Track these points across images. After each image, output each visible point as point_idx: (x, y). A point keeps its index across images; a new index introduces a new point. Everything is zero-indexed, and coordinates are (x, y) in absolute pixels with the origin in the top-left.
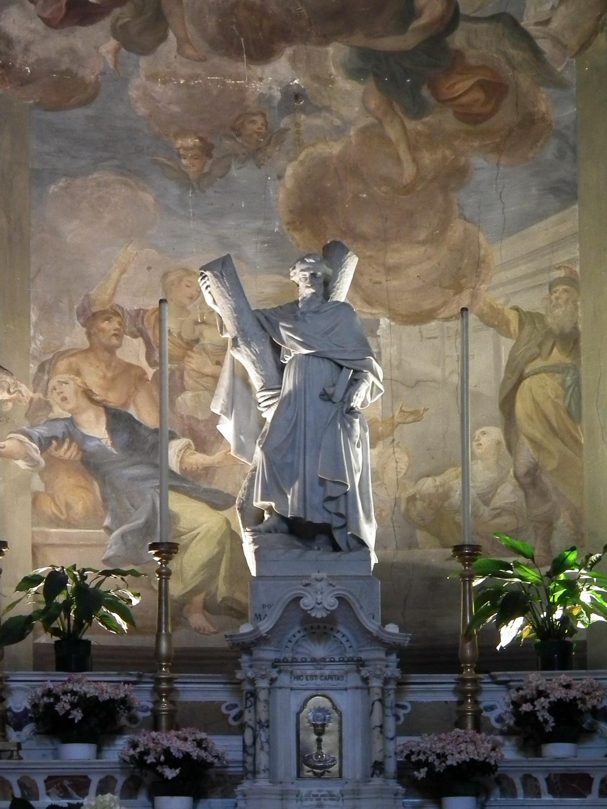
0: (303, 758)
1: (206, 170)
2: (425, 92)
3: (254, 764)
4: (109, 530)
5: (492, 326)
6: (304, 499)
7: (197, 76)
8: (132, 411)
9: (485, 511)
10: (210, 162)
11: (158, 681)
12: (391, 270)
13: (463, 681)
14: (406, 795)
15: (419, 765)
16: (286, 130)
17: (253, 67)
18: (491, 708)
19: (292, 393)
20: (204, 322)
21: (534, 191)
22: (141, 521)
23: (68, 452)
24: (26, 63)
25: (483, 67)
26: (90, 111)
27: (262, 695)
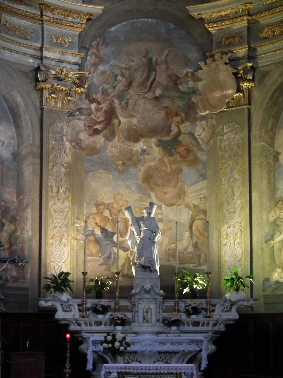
0: (144, 318)
1: (124, 169)
2: (173, 151)
3: (135, 319)
4: (101, 257)
5: (188, 208)
6: (145, 261)
7: (122, 146)
8: (106, 228)
9: (185, 253)
10: (124, 167)
11: (116, 301)
12: (165, 193)
13: (175, 302)
14: (164, 326)
15: (166, 320)
16: (141, 159)
17: (135, 144)
18: (181, 307)
20: (123, 206)
21: (197, 175)
22: (108, 255)
23: (92, 238)
25: (187, 145)
26: (98, 155)
27: (136, 305)
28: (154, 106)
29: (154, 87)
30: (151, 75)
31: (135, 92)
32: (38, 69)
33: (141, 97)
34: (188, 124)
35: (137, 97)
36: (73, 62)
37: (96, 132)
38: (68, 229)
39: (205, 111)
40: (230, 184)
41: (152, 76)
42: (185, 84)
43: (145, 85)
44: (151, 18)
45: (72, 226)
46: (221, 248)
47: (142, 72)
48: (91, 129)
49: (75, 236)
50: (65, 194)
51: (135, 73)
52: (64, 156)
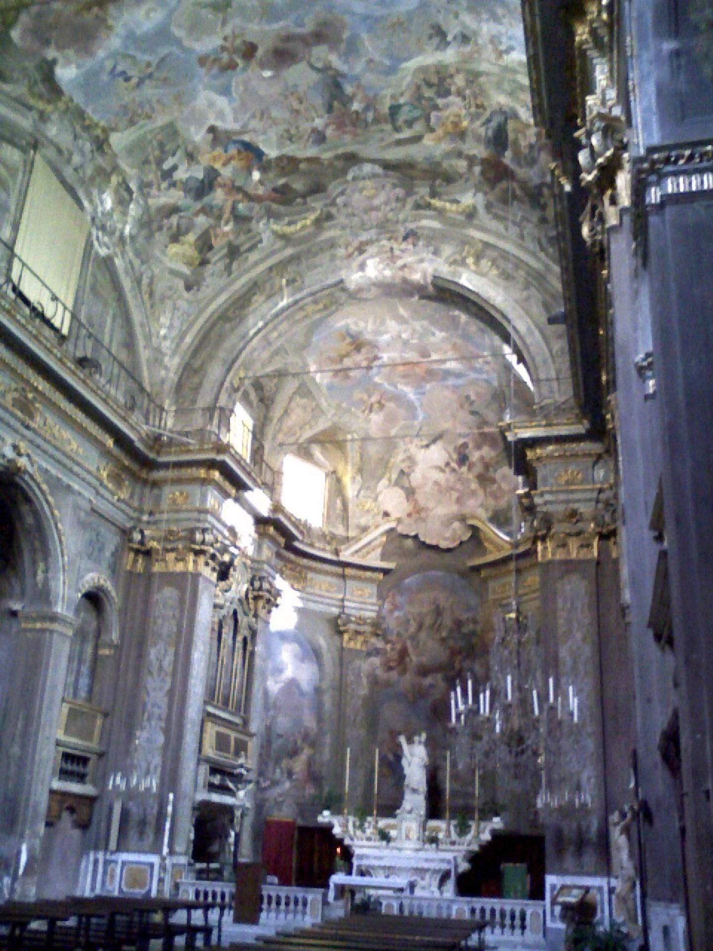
32: (339, 617)
37: (390, 669)
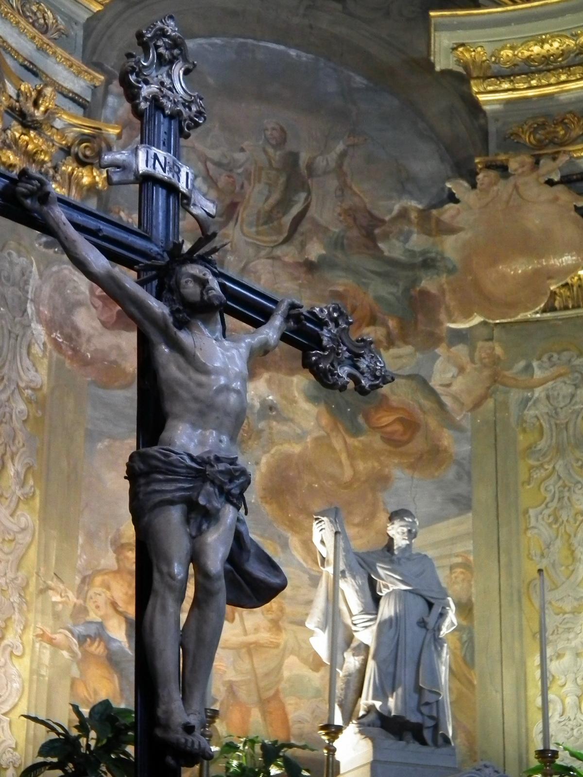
16: (262, 431)
19: (394, 619)
21: (439, 499)
23: (97, 648)
24: (88, 350)
28: (300, 285)
29: (302, 234)
30: (296, 198)
31: (244, 234)
33: (263, 253)
34: (408, 349)
35: (251, 251)
36: (70, 91)
38: (26, 603)
39: (468, 315)
40: (558, 529)
41: (296, 202)
42: (398, 239)
43: (275, 223)
44: (297, 47)
45: (38, 596)
46: (526, 717)
47: (270, 185)
48: (111, 310)
49: (48, 631)
50: (23, 485)
51: (246, 183)
52: (27, 363)
